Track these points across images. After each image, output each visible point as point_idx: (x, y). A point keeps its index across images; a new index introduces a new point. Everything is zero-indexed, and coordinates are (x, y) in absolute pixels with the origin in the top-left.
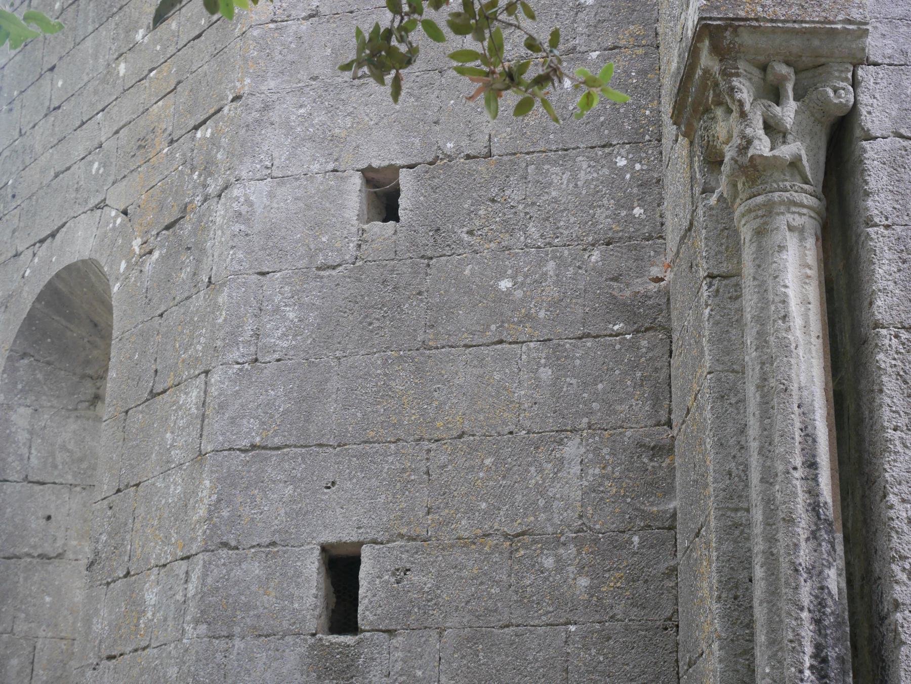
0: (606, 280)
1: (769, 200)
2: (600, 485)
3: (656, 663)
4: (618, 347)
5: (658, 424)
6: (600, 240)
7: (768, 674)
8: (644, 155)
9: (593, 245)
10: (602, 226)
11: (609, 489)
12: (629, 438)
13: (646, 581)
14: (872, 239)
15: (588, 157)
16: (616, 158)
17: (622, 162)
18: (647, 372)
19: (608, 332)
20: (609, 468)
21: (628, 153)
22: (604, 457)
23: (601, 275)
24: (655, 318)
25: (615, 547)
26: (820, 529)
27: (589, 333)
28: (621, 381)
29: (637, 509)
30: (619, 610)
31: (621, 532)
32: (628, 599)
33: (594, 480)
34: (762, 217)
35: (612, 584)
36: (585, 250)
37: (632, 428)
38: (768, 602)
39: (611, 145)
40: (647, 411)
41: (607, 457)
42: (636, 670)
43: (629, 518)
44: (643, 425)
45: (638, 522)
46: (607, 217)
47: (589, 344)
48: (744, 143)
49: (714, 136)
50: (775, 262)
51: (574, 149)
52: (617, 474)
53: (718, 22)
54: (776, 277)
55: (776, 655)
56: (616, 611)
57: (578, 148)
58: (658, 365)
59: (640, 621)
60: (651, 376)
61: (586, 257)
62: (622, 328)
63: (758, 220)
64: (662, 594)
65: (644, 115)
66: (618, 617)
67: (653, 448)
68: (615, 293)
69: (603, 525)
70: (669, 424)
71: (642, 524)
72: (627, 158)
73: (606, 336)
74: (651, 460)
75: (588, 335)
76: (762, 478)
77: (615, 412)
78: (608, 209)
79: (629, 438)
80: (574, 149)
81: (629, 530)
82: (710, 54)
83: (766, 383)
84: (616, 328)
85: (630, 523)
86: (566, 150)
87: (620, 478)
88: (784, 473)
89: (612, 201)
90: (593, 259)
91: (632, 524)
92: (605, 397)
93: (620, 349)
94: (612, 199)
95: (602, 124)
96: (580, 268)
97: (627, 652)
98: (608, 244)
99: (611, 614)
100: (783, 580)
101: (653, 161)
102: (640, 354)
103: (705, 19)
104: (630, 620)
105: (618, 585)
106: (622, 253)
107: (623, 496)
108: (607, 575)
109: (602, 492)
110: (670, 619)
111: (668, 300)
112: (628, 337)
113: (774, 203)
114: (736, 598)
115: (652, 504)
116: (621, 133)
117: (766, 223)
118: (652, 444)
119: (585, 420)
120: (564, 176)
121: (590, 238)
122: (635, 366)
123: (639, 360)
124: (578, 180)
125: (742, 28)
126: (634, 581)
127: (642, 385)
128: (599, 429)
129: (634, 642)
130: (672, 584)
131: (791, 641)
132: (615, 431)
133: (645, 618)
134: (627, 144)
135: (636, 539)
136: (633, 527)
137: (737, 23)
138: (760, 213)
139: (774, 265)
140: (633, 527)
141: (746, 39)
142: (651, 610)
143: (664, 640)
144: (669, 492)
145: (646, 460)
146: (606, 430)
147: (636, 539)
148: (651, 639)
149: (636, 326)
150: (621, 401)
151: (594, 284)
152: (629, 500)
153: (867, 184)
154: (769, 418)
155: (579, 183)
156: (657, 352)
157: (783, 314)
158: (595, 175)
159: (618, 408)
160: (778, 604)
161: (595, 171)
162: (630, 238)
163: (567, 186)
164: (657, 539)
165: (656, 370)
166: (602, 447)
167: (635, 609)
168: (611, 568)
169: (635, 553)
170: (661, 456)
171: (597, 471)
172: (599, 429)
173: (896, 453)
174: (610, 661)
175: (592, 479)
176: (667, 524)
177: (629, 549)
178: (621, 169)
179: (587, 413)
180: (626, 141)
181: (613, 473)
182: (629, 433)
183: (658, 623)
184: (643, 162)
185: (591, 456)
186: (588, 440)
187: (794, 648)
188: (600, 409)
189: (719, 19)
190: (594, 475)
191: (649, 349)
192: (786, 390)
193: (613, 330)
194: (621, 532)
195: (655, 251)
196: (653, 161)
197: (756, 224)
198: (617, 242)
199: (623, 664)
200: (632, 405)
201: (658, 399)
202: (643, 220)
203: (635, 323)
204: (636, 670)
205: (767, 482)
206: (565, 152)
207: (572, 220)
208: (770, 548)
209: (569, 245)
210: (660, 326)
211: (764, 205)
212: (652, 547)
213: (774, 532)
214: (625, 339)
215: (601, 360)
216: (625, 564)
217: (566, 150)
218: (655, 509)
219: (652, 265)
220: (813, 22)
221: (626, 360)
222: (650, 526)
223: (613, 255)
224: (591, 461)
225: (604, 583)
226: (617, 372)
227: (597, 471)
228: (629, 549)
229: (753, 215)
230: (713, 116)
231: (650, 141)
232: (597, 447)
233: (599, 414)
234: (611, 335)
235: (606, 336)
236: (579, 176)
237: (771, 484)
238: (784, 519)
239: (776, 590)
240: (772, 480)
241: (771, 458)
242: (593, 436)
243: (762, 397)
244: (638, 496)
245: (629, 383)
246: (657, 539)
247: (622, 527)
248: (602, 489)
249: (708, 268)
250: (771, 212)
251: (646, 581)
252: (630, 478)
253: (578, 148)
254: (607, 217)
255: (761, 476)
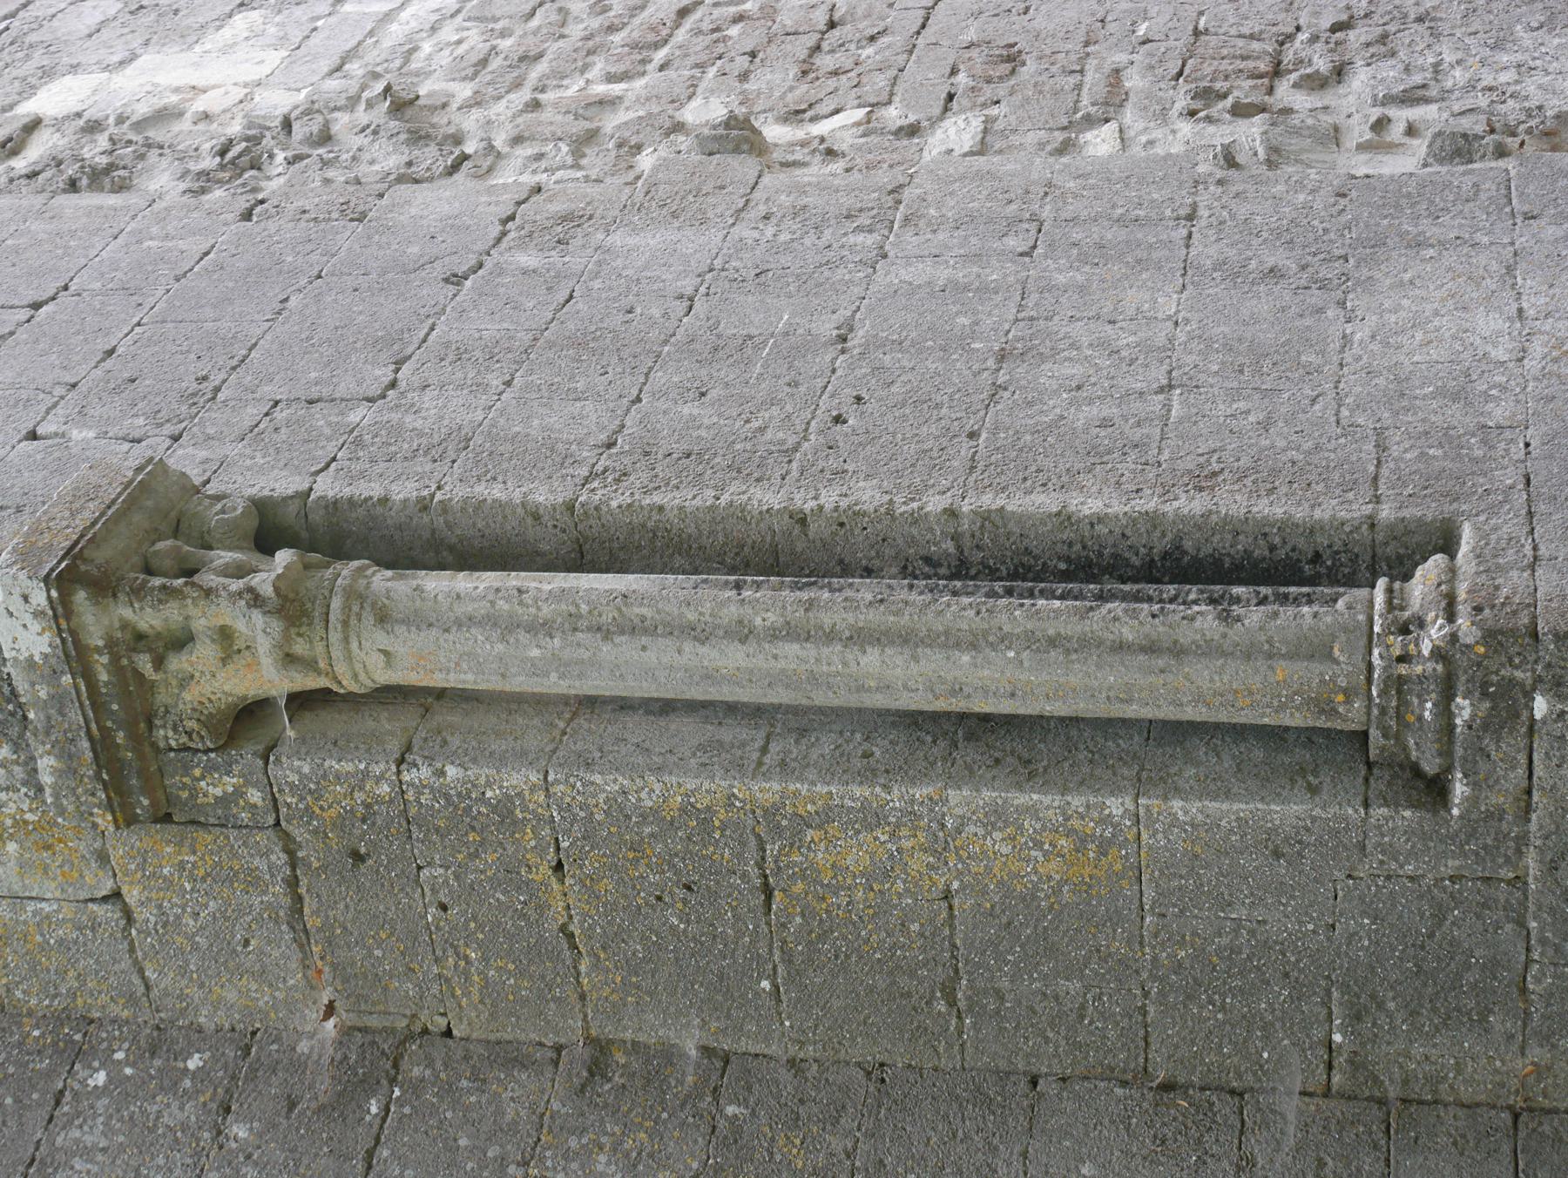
0: (288, 1118)
1: (344, 589)
2: (627, 1155)
3: (933, 1098)
4: (407, 1110)
5: (556, 1063)
6: (216, 1121)
7: (1017, 653)
8: (105, 1045)
9: (219, 1133)
10: (193, 1118)
11: (638, 1143)
12: (564, 1106)
13: (802, 1101)
14: (450, 500)
15: (64, 1128)
16: (87, 1085)
17: (101, 1078)
18: (464, 1071)
19: (378, 1121)
20: (604, 1140)
21: (90, 1067)
22: (583, 1146)
23: (275, 1126)
24: (383, 1053)
25: (736, 1141)
26: (829, 583)
27: (367, 1152)
28: (467, 1109)
29: (683, 1105)
30: (838, 1144)
31: (713, 1132)
32: (824, 1130)
33: (616, 1164)
34: (362, 607)
35: (795, 1151)
36: (221, 1147)
37: (548, 1101)
38: (917, 646)
39: (61, 1092)
40: (529, 1076)
41: (585, 1141)
42: (940, 1127)
43: (694, 1117)
44: (550, 1084)
45: (703, 1105)
46: (181, 1108)
47: (386, 1153)
48: (248, 596)
49: (194, 710)
50: (435, 597)
51: (37, 1149)
52: (616, 1129)
53: (63, 565)
54: (458, 596)
55: (992, 644)
56: (840, 1148)
57: (39, 1142)
58: (460, 1053)
59: (863, 1115)
60: (474, 1066)
61: (234, 1145)
62: (379, 1101)
63: (364, 614)
64: (827, 1080)
65: (37, 1039)
66: (849, 1146)
67: (592, 1074)
68: (314, 1105)
69: (693, 1156)
70: (558, 1049)
71: (709, 1099)
72: (97, 1070)
73: (381, 1127)
74: (609, 1080)
75: (370, 1154)
76: (740, 641)
77: (514, 1122)
78: (168, 1105)
79: (564, 1106)
80: (37, 1149)
81: (713, 1119)
82: (97, 603)
83: (604, 628)
84: (374, 1110)
85: (702, 1116)
86: (33, 1160)
87: (625, 1126)
88: (742, 605)
89: (158, 1099)
90: (242, 1134)
91: (705, 1114)
92: (483, 1137)
93: (413, 1107)
94: (154, 1098)
95: (17, 1101)
96: (248, 1157)
97: (909, 1138)
98: (228, 1110)
99: (843, 1156)
100: (892, 618)
101: (122, 1032)
102: (432, 1078)
103: (48, 575)
104: (859, 1130)
105: (798, 1142)
106: (254, 1091)
107: (656, 1123)
108: (778, 1157)
109: (639, 1154)
110: (869, 1074)
111: (360, 1030)
112: (397, 1093)
113: (351, 586)
114: (887, 771)
115: (681, 1082)
116: (50, 1074)
117: (374, 604)
118: (585, 1074)
119: (512, 1169)
120: (77, 1167)
121: (206, 1135)
122: (449, 1090)
123: (442, 1081)
124: (95, 1145)
125: (86, 551)
126: (798, 1119)
127: (484, 1081)
128: (533, 1149)
129: (895, 1126)
130: (815, 1067)
131: (978, 613)
132: (545, 1126)
133: (860, 1107)
134: (72, 1067)
135: (731, 1110)
136: (710, 1113)
137: (77, 549)
138: (356, 608)
139: (439, 597)
140: (710, 1113)
141: (101, 555)
142: (850, 1098)
143: (900, 1083)
144: (669, 1054)
145: (607, 1087)
146: (539, 1140)
147: (731, 1110)
148: (895, 1102)
149: (384, 1082)
150: (499, 1112)
151: (286, 1137)
152: (665, 1115)
153: (371, 498)
154: (656, 627)
155: (101, 1146)
156: (439, 1056)
157: (515, 592)
158: (101, 1119)
159: (508, 1118)
160: (921, 635)
161: (94, 1119)
162: (234, 1078)
163: (97, 1163)
164: (738, 1080)
165: (466, 1058)
166: (566, 1147)
167: (843, 1121)
168: (768, 1150)
169: (753, 1113)
170: (607, 1066)
171: (603, 1158)
172: (533, 1149)
173: (749, 499)
174: (919, 1165)
175: (613, 1167)
176: (719, 1064)
177: (745, 1120)
178: (110, 1080)
179: (502, 1164)
180: (68, 1068)
181: (614, 1134)
182: (555, 1105)
183: (871, 1089)
184: (115, 1048)
185: (574, 1166)
186: (547, 1168)
187: (987, 610)
188: (501, 1146)
189: (59, 563)
190: (608, 1163)
191: (430, 1064)
192: (625, 596)
193: (377, 1115)
194: (713, 1132)
195: (273, 1042)
196: (122, 1032)
197: (369, 619)
198: (231, 1096)
199: (927, 1144)
200: (512, 1099)
201: (516, 1059)
202: (213, 1056)
203: (378, 1082)
204: (940, 1127)
205: (747, 637)
206: (36, 1163)
207: (161, 1161)
208: (841, 640)
209: (202, 1170)
210: (397, 1048)
211: (348, 599)
212: (749, 1089)
213: (820, 633)
214: (398, 1098)
215: (419, 1137)
216: (766, 1129)
217: (33, 1160)
218: (690, 1079)
219: (294, 1049)
220: (120, 494)
221: (435, 1100)
222: (715, 1089)
223: (250, 1105)
224: (582, 1167)
225: (790, 1164)
226: (449, 1115)
227: (603, 1158)
228: (745, 1120)
229: (353, 621)
230: (162, 709)
231: (85, 1035)
232: (563, 1156)
233: (509, 1147)
234: (384, 1120)
235: (381, 1127)
236: (89, 1145)
237: (751, 632)
238: (807, 610)
239: (901, 636)
240: (746, 631)
241: (714, 629)
242: (542, 1159)
243: (622, 633)
244: (663, 1101)
245: (473, 1099)
246: (738, 1080)
247: (707, 1129)
248: (634, 1154)
249: (387, 762)
250: (360, 596)
251: (802, 1101)
252: (630, 1110)
253: (39, 1142)
254: (181, 1108)
255: (736, 642)
